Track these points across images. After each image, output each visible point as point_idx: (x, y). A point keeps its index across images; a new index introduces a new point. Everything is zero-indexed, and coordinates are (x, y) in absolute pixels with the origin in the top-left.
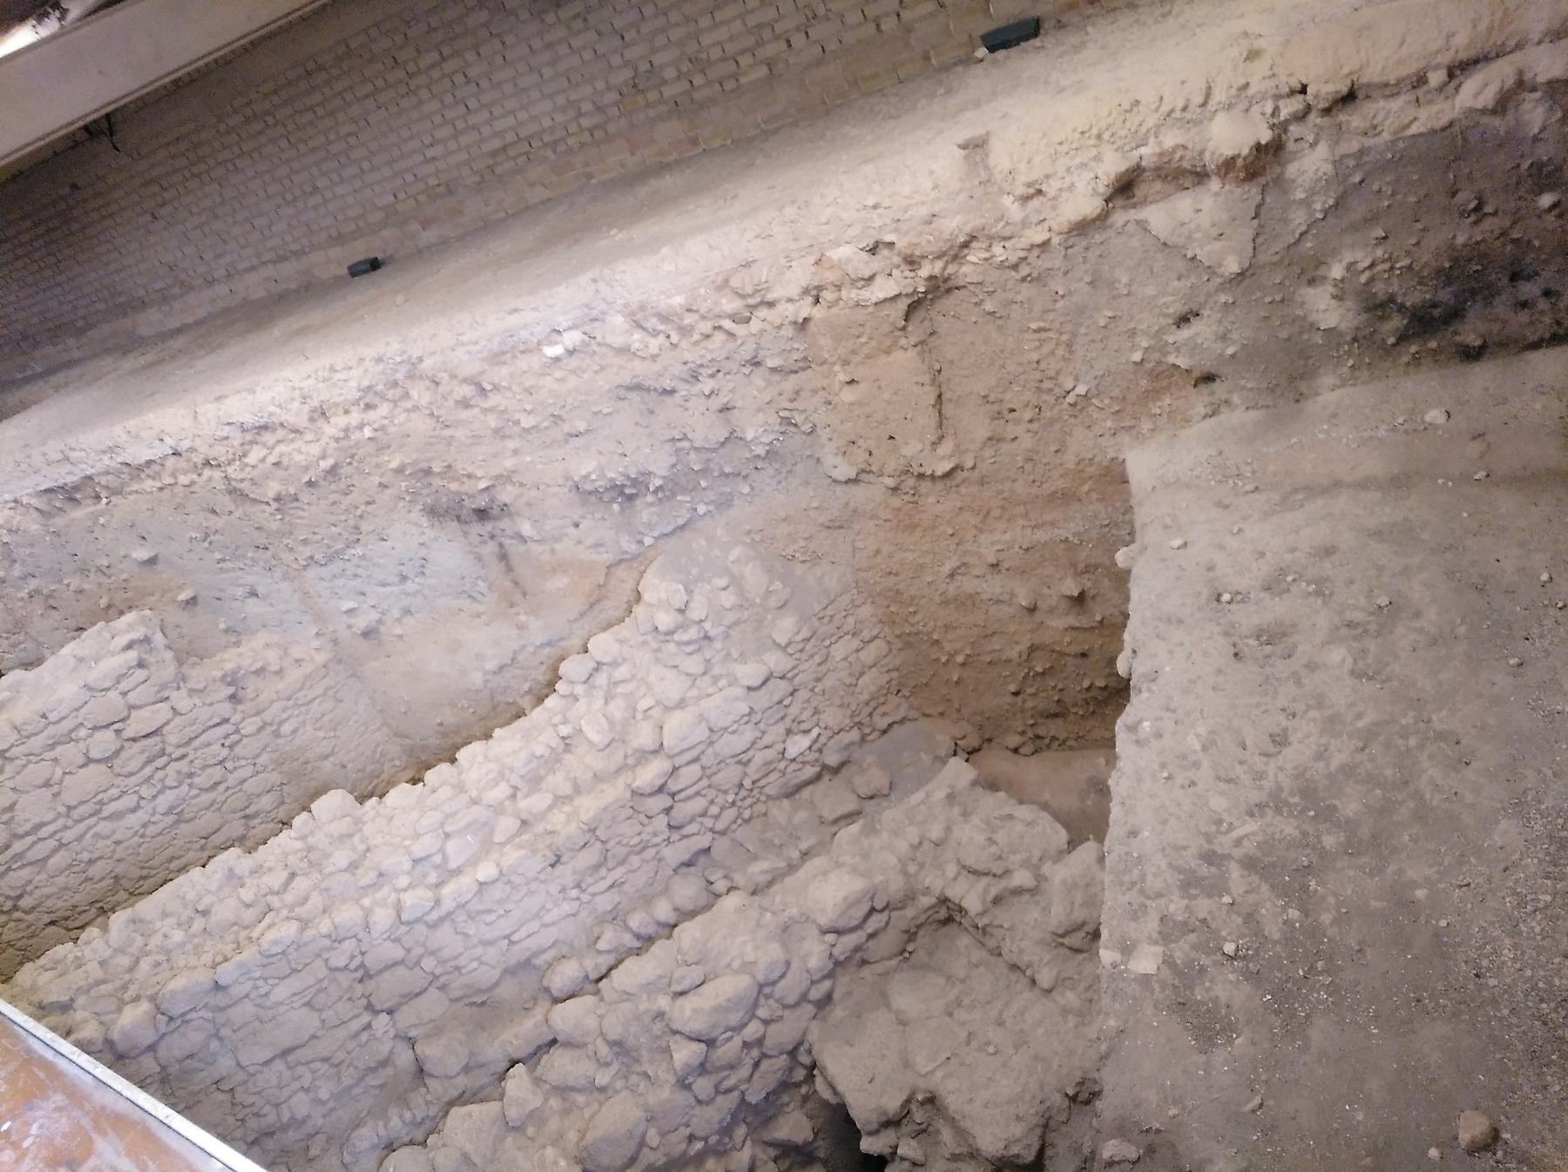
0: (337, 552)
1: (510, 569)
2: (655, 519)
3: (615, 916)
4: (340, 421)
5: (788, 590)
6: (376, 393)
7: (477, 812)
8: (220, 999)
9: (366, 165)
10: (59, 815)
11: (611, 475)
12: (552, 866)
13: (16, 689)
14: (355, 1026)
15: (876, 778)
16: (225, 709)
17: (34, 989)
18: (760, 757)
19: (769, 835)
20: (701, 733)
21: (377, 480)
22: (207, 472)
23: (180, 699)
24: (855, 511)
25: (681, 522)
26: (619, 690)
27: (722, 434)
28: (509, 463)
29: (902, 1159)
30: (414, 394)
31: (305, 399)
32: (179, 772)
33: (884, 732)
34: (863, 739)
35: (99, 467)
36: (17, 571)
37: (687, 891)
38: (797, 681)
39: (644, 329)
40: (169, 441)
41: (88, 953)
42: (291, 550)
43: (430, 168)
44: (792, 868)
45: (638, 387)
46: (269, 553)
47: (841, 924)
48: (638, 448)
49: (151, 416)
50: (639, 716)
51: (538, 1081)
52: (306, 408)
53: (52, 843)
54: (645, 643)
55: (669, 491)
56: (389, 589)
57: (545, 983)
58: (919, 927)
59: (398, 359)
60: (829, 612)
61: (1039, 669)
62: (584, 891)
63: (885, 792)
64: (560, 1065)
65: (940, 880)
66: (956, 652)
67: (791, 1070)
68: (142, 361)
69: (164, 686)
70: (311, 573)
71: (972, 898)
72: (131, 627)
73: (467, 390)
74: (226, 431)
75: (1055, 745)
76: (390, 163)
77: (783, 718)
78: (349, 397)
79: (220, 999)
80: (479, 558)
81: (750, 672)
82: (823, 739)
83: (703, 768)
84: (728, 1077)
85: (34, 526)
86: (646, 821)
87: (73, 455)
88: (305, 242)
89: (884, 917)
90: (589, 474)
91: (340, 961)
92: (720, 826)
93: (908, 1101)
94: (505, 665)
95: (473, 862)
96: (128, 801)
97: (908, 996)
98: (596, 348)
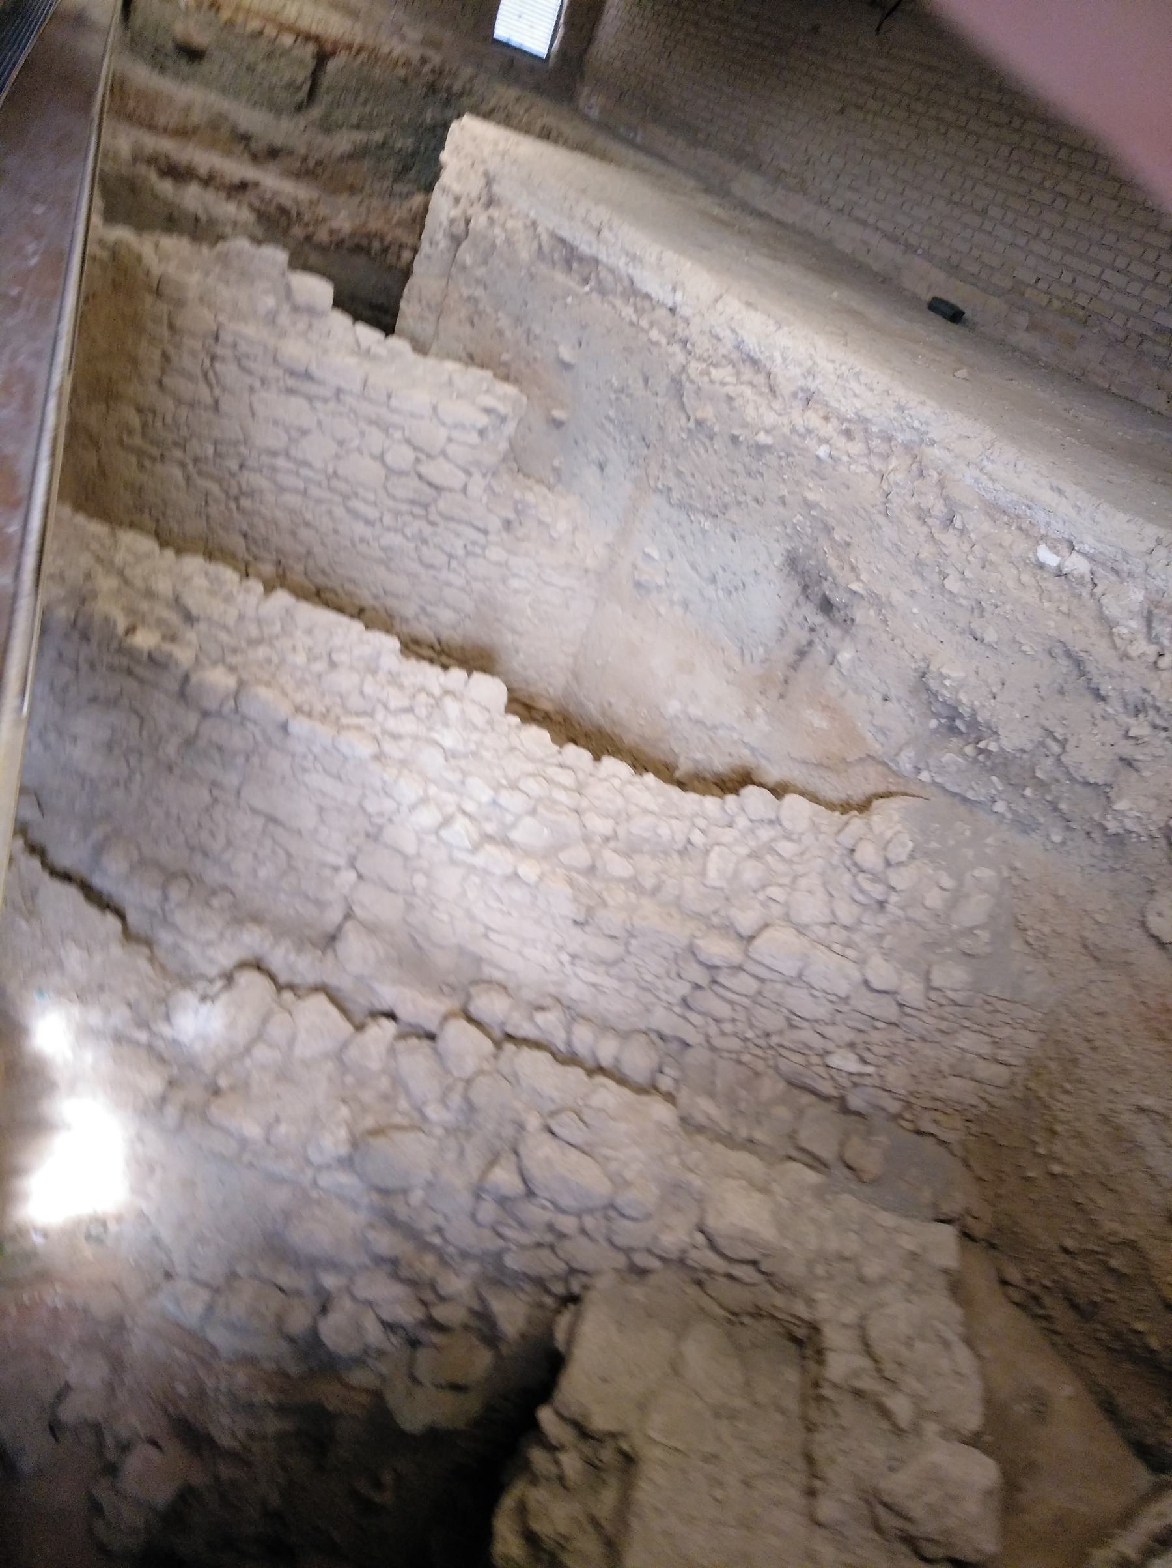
0: (691, 506)
1: (794, 667)
2: (953, 768)
3: (573, 1013)
4: (813, 419)
5: (988, 949)
6: (866, 430)
7: (571, 824)
8: (277, 737)
9: (1046, 234)
10: (325, 471)
11: (964, 698)
12: (576, 922)
13: (394, 355)
14: (331, 858)
15: (871, 1160)
16: (495, 524)
17: (187, 580)
18: (807, 1035)
19: (743, 1093)
20: (789, 968)
21: (785, 492)
22: (676, 348)
23: (477, 486)
24: (1128, 964)
25: (970, 795)
26: (769, 858)
27: (1098, 775)
28: (897, 596)
29: (557, 1463)
30: (893, 463)
31: (810, 373)
32: (420, 531)
33: (919, 1132)
34: (896, 1117)
35: (612, 261)
36: (480, 272)
37: (638, 1060)
38: (907, 1020)
39: (1149, 626)
40: (679, 297)
41: (240, 598)
42: (663, 467)
43: (1093, 287)
44: (729, 1140)
45: (1078, 663)
46: (645, 451)
47: (722, 1243)
48: (1012, 705)
49: (689, 264)
50: (761, 896)
51: (392, 1052)
52: (801, 382)
53: (301, 485)
54: (831, 849)
55: (994, 764)
56: (692, 573)
57: (473, 990)
58: (773, 1317)
59: (916, 424)
60: (999, 1005)
61: (1114, 1263)
62: (573, 964)
63: (866, 1178)
64: (416, 1062)
65: (833, 1313)
66: (1059, 1160)
67: (557, 1277)
68: (716, 211)
69: (478, 463)
70: (657, 500)
71: (842, 1363)
72: (504, 398)
73: (939, 509)
74: (725, 334)
75: (1045, 1324)
76: (1066, 250)
77: (860, 1031)
78: (843, 409)
79: (277, 737)
80: (783, 632)
81: (882, 973)
82: (867, 1081)
83: (760, 993)
84: (510, 1226)
85: (525, 254)
86: (673, 974)
87: (606, 233)
88: (925, 244)
89: (756, 1277)
90: (948, 677)
91: (371, 806)
92: (718, 1042)
93: (613, 1435)
94: (703, 724)
95: (528, 853)
96: (372, 513)
97: (700, 1352)
98: (1085, 594)
